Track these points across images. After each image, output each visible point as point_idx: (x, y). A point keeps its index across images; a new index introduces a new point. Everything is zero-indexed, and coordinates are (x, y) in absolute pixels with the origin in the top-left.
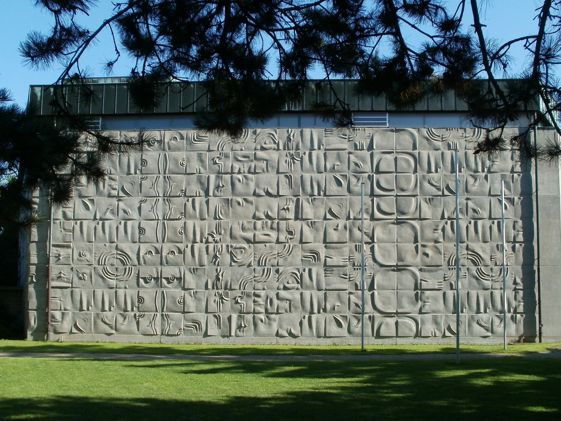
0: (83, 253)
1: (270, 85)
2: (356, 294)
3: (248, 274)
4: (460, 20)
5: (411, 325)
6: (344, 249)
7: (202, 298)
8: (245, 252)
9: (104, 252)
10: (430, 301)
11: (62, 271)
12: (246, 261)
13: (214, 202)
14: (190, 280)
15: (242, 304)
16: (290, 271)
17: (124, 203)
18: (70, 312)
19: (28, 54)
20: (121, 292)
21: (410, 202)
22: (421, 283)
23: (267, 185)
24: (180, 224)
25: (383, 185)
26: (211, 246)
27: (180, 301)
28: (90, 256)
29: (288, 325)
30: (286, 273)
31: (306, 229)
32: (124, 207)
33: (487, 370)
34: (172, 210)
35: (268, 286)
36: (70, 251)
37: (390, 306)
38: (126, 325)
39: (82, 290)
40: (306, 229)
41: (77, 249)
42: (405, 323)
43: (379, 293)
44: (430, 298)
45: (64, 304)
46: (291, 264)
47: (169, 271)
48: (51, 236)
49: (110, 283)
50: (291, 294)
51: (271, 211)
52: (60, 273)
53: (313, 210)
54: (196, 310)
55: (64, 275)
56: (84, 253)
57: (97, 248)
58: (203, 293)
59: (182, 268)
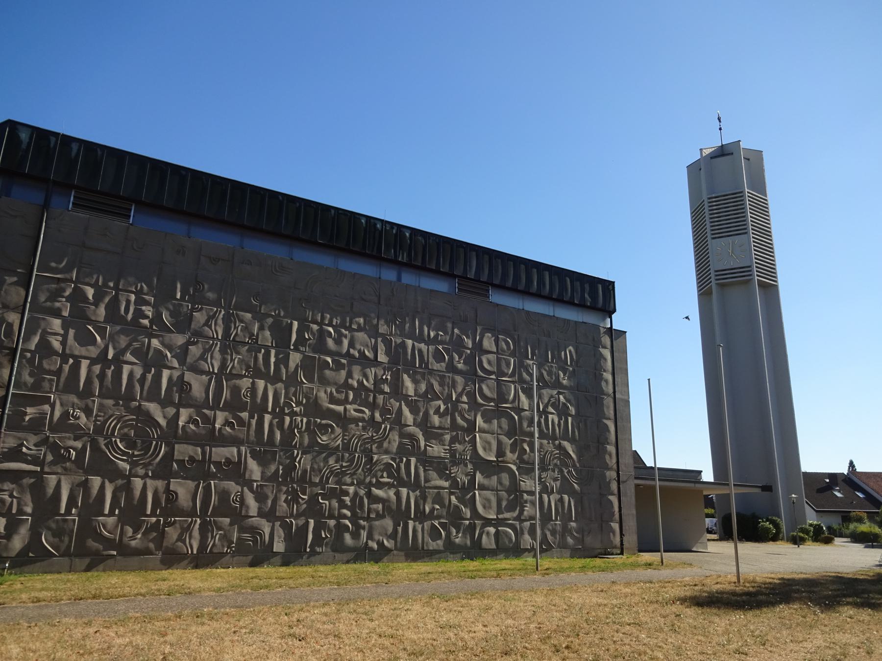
0: (73, 413)
1: (375, 225)
2: (457, 495)
3: (333, 462)
4: (835, 545)
5: (511, 534)
6: (445, 436)
7: (270, 494)
8: (331, 432)
9: (114, 415)
10: (528, 505)
11: (25, 442)
12: (333, 443)
13: (295, 358)
14: (254, 469)
15: (324, 505)
16: (385, 461)
17: (159, 341)
18: (30, 518)
19: (723, 152)
20: (138, 483)
21: (510, 387)
22: (520, 483)
23: (363, 346)
24: (246, 383)
25: (486, 365)
26: (287, 419)
27: (236, 499)
28: (87, 419)
29: (380, 534)
30: (380, 462)
31: (406, 411)
32: (157, 345)
33: (500, 267)
34: (236, 362)
35: (359, 480)
36: (47, 408)
37: (490, 511)
38: (140, 538)
39: (63, 477)
40: (406, 411)
41: (62, 405)
42: (506, 533)
43: (479, 494)
44: (528, 502)
45: (19, 504)
46: (387, 452)
47: (221, 453)
48: (13, 378)
49: (120, 466)
50: (386, 492)
51: (367, 380)
52: (22, 445)
53: (414, 385)
54: (258, 513)
55: (28, 448)
56: (75, 413)
57: (101, 407)
58: (271, 487)
59: (243, 449)
